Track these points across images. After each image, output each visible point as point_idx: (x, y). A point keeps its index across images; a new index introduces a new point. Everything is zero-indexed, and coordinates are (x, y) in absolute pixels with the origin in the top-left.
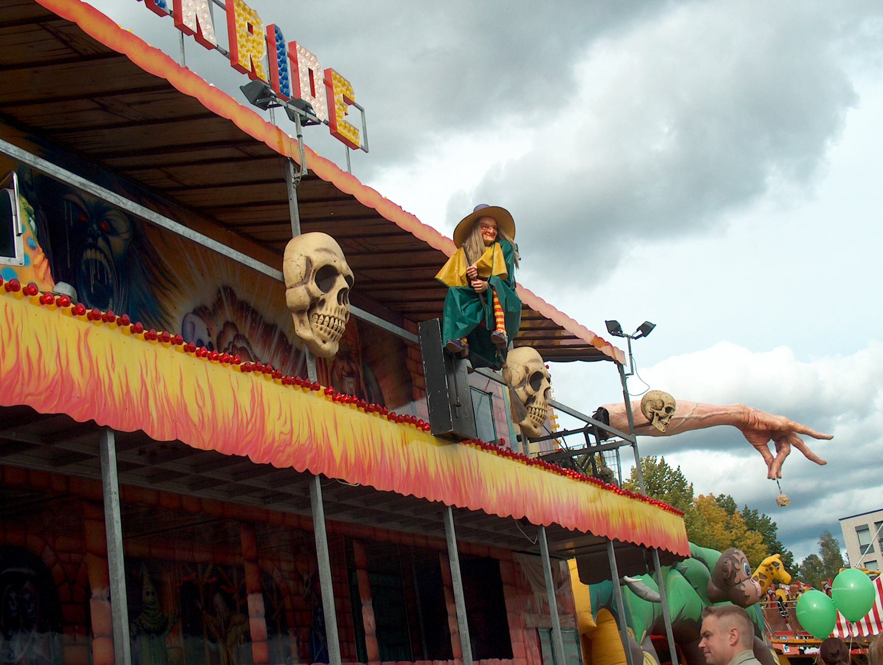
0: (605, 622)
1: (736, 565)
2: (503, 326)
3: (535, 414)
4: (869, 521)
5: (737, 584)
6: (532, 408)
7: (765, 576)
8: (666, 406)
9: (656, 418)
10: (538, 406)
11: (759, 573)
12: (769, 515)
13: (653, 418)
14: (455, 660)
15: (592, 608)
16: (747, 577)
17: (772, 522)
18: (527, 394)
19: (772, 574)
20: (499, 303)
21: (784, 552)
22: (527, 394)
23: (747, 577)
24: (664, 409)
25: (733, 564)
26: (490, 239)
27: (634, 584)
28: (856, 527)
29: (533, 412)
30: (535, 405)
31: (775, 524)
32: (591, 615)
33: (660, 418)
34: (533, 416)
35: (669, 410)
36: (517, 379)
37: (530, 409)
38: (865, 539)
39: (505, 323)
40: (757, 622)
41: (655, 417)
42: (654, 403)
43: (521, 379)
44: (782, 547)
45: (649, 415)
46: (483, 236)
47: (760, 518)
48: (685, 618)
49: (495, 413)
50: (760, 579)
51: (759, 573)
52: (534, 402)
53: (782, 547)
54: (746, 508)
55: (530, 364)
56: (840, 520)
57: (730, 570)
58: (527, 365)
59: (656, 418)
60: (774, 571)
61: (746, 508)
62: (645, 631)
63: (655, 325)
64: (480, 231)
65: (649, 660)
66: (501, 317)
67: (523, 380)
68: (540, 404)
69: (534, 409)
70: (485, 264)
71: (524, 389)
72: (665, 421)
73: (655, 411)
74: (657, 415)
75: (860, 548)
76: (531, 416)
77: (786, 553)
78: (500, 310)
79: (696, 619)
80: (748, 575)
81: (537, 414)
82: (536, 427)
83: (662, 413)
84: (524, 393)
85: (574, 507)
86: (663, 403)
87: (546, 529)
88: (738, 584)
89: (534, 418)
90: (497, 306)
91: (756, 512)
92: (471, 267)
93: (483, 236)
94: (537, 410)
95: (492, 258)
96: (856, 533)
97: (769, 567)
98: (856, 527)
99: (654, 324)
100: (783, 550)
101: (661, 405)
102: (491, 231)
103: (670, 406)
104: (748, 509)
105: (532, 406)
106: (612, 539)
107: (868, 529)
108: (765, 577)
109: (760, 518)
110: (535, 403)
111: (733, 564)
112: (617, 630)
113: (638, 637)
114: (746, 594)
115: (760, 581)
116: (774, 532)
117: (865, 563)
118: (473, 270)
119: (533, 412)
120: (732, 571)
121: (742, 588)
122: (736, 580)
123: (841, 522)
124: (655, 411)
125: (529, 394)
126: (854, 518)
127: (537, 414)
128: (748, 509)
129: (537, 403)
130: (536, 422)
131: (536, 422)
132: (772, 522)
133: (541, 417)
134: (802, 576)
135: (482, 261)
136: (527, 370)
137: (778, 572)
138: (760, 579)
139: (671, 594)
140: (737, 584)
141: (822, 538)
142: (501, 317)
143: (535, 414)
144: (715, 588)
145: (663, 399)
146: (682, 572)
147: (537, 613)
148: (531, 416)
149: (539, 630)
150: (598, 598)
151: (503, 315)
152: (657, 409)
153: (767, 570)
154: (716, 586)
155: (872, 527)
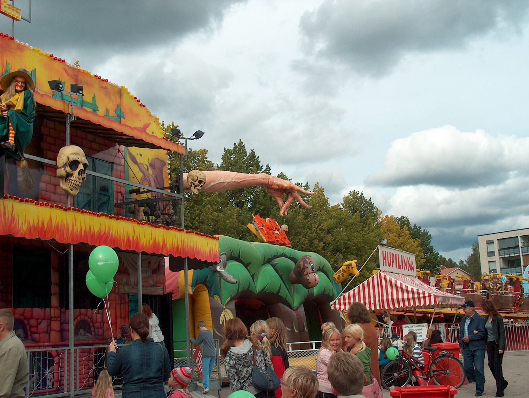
0: (202, 291)
1: (306, 265)
2: (13, 139)
3: (71, 183)
4: (495, 238)
5: (305, 275)
6: (70, 180)
7: (345, 271)
8: (199, 179)
9: (193, 186)
10: (74, 179)
11: (342, 269)
12: (427, 230)
13: (192, 185)
14: (52, 309)
15: (192, 284)
16: (312, 272)
17: (429, 234)
18: (66, 172)
19: (349, 270)
20: (12, 126)
21: (434, 252)
22: (66, 172)
23: (312, 272)
24: (197, 181)
25: (304, 264)
26: (19, 89)
27: (222, 272)
28: (486, 241)
29: (70, 182)
30: (72, 178)
31: (430, 235)
32: (191, 287)
33: (196, 186)
34: (70, 184)
35: (200, 182)
36: (62, 163)
37: (69, 180)
38: (491, 248)
39: (15, 137)
40: (333, 295)
41: (193, 185)
42: (193, 177)
43: (64, 163)
44: (433, 249)
45: (190, 183)
46: (15, 86)
47: (422, 232)
48: (267, 292)
49: (114, 173)
50: (342, 273)
51: (342, 269)
52: (72, 176)
53: (433, 249)
54: (415, 225)
55: (70, 156)
56: (478, 236)
57: (302, 267)
58: (69, 156)
59: (193, 186)
60: (350, 269)
61: (415, 225)
62: (229, 298)
63: (204, 133)
64: (14, 84)
65: (228, 314)
66: (13, 133)
67: (65, 164)
68: (75, 178)
69: (71, 180)
70: (12, 103)
71: (65, 169)
72: (198, 188)
73: (193, 182)
74: (194, 184)
75: (488, 253)
76: (69, 184)
77: (435, 253)
78: (12, 130)
79: (275, 293)
80: (313, 271)
81: (73, 183)
82: (72, 190)
83: (197, 183)
84: (64, 171)
85: (105, 234)
86: (198, 178)
87: (74, 246)
88: (306, 275)
89: (71, 185)
90: (11, 128)
91: (420, 227)
92: (2, 104)
93: (15, 86)
94: (73, 181)
95: (17, 100)
96: (486, 244)
97: (349, 266)
98: (486, 241)
99: (203, 132)
100: (434, 251)
101: (197, 178)
102: (20, 84)
103: (201, 180)
104: (416, 226)
105: (70, 179)
106: (140, 252)
107: (493, 243)
108: (345, 271)
109: (422, 232)
110: (72, 177)
111: (304, 264)
112: (208, 296)
113: (223, 301)
114: (309, 281)
115: (342, 274)
116: (430, 240)
117: (489, 262)
118: (2, 106)
119: (70, 182)
120: (303, 268)
121: (308, 278)
122: (305, 273)
123: (479, 237)
124: (193, 182)
125: (67, 172)
126: (503, 233)
127: (73, 183)
128: (416, 226)
129: (73, 177)
130: (72, 188)
131: (72, 188)
132: (429, 234)
133: (77, 186)
134: (467, 265)
135: (10, 101)
136: (68, 158)
137: (352, 269)
138: (342, 273)
139: (260, 278)
140: (305, 275)
141: (474, 246)
142: (13, 133)
143: (71, 183)
144: (294, 276)
145: (198, 176)
146: (274, 266)
147: (131, 285)
148: (69, 184)
149: (129, 295)
150: (197, 278)
151: (14, 132)
152: (194, 181)
153: (346, 268)
154: (295, 275)
155: (496, 242)
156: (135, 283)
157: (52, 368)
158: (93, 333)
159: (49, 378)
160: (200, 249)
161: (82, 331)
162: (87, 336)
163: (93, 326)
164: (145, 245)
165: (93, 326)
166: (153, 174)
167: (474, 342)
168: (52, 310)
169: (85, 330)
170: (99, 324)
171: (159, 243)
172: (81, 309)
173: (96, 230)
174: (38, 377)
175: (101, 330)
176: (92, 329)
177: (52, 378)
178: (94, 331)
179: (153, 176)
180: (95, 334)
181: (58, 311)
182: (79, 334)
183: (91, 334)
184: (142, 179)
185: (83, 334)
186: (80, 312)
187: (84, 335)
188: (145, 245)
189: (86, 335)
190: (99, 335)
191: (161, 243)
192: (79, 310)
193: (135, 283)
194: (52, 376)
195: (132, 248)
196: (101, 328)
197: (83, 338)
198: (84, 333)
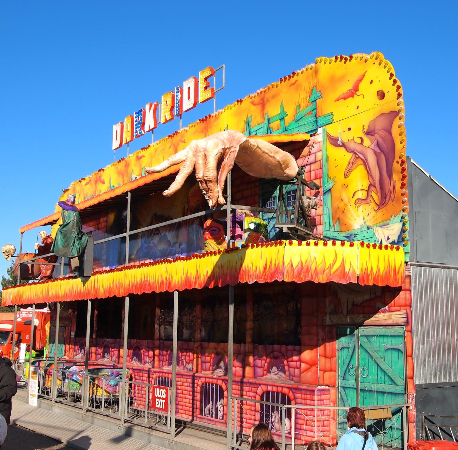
85: (144, 281)
156: (349, 309)
157: (222, 400)
158: (287, 373)
159: (220, 409)
160: (248, 267)
161: (274, 369)
162: (281, 375)
163: (288, 365)
164: (176, 283)
165: (288, 365)
166: (372, 143)
167: (76, 434)
168: (247, 345)
169: (278, 369)
170: (295, 363)
171: (191, 276)
172: (274, 345)
173: (139, 279)
174: (212, 406)
175: (297, 371)
176: (286, 368)
177: (222, 410)
178: (289, 371)
179: (373, 146)
180: (290, 374)
181: (251, 346)
182: (272, 372)
183: (285, 373)
184: (351, 162)
185: (276, 373)
186: (273, 348)
187: (277, 374)
188: (176, 283)
189: (279, 374)
190: (294, 376)
191: (194, 276)
192: (271, 346)
193: (349, 309)
194: (222, 408)
195: (166, 289)
196: (297, 368)
197: (276, 377)
198: (277, 372)
